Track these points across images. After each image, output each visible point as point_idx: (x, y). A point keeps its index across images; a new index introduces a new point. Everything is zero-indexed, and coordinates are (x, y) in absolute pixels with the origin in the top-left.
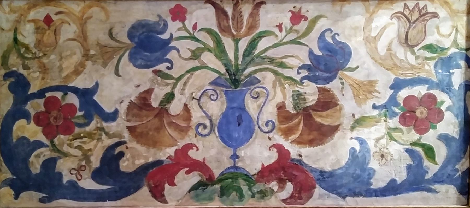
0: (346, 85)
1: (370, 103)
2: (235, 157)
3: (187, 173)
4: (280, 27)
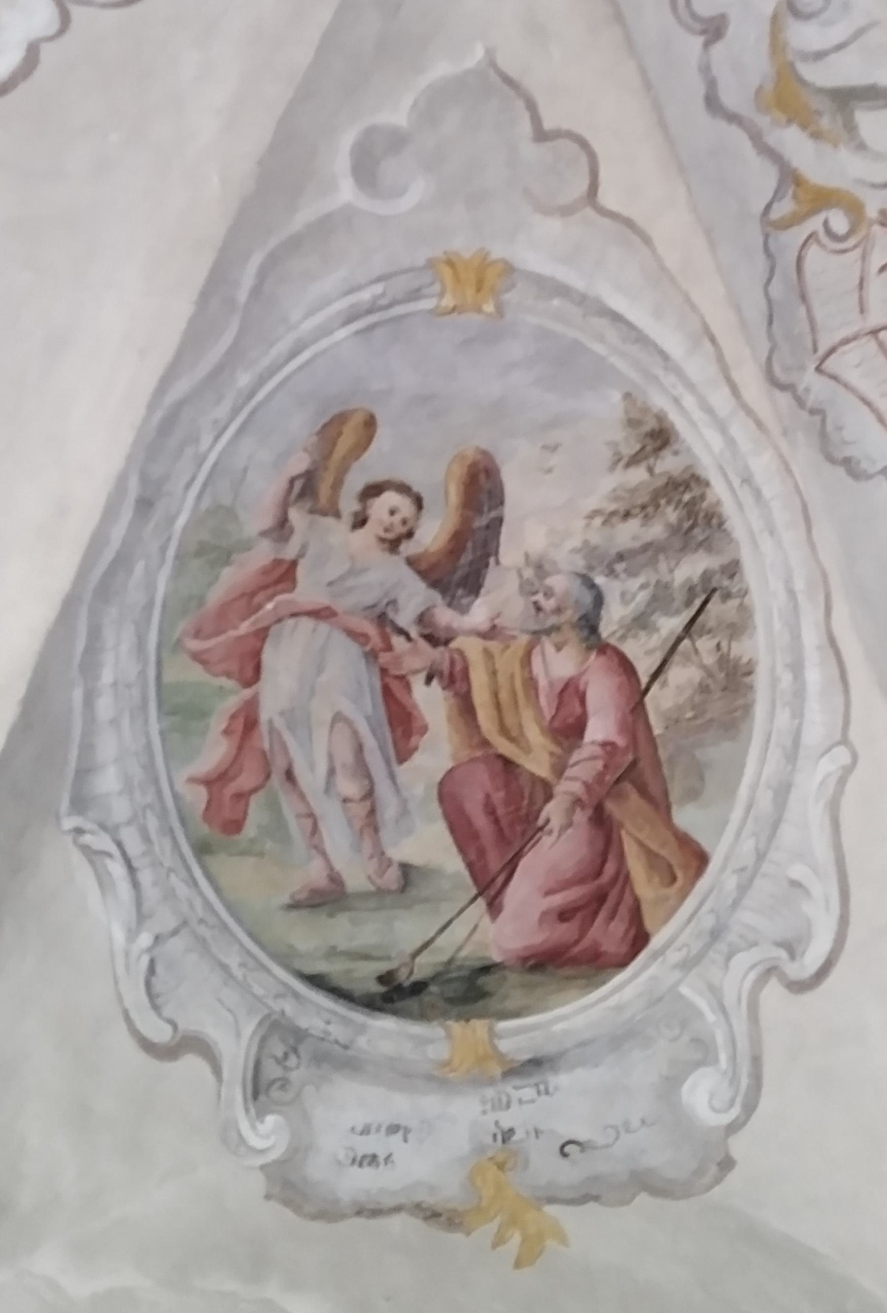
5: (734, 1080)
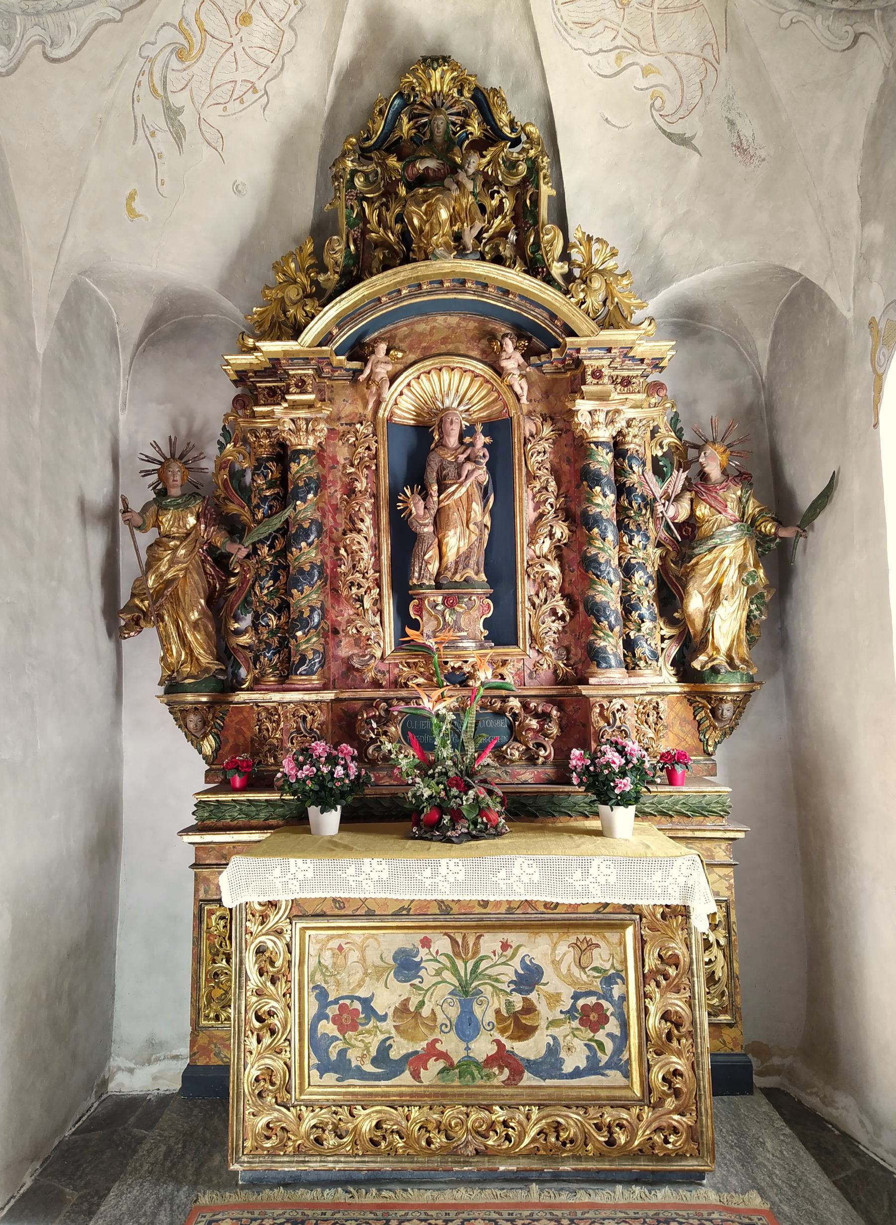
0: (541, 995)
1: (559, 1009)
2: (468, 1049)
3: (436, 1060)
4: (494, 952)
5: (10, 60)
